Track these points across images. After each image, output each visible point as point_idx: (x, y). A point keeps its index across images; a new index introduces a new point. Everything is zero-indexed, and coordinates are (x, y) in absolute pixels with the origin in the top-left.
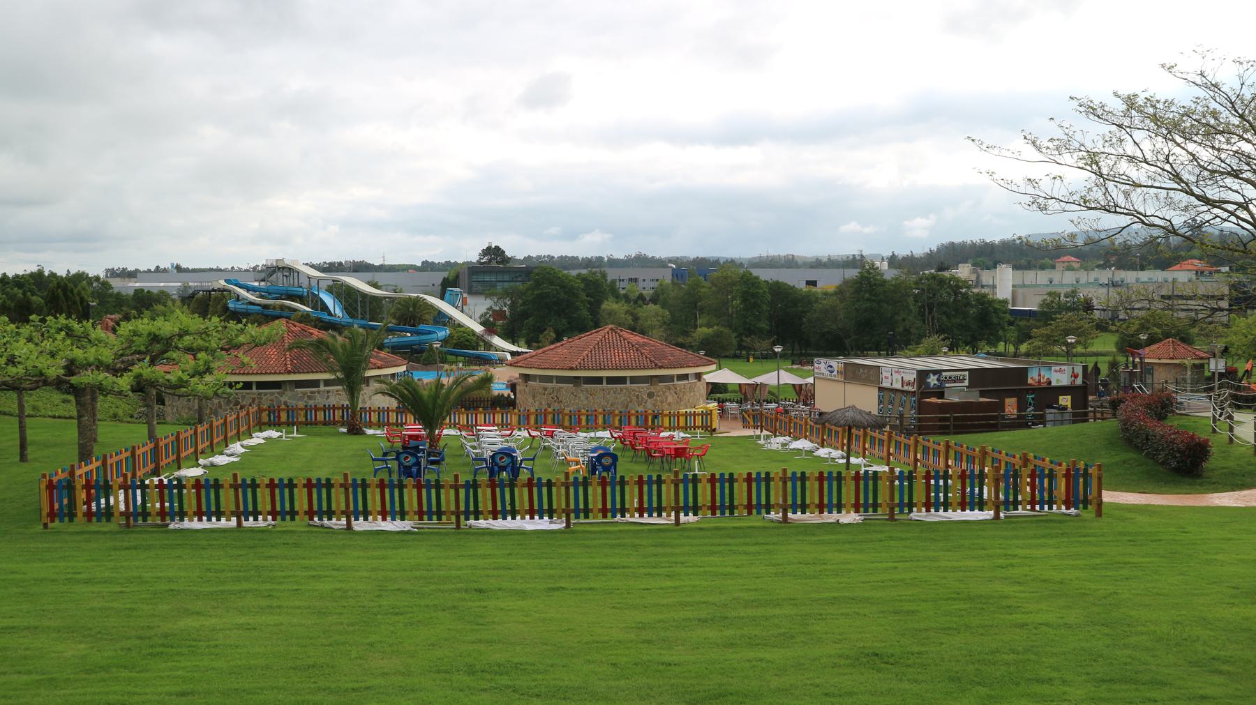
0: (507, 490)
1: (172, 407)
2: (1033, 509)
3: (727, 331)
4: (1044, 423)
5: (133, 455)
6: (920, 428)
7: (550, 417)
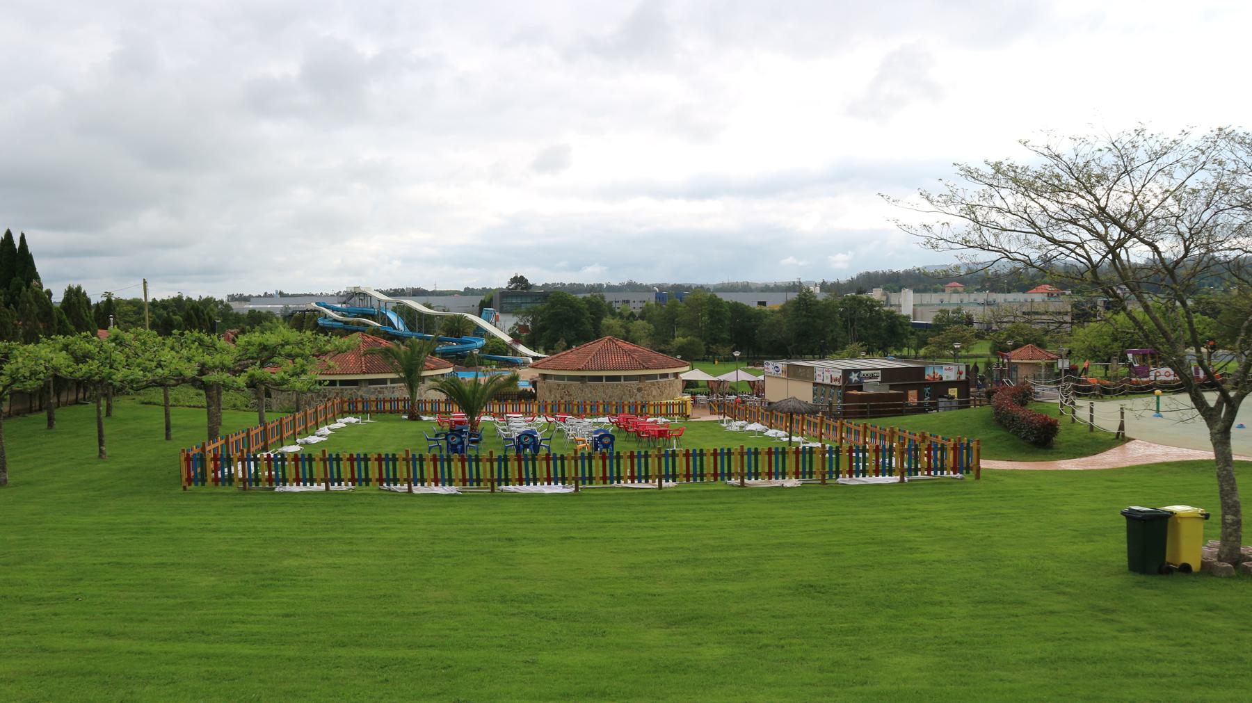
0: (530, 463)
1: (277, 399)
2: (929, 474)
3: (697, 340)
4: (937, 409)
5: (248, 434)
6: (845, 413)
7: (562, 407)
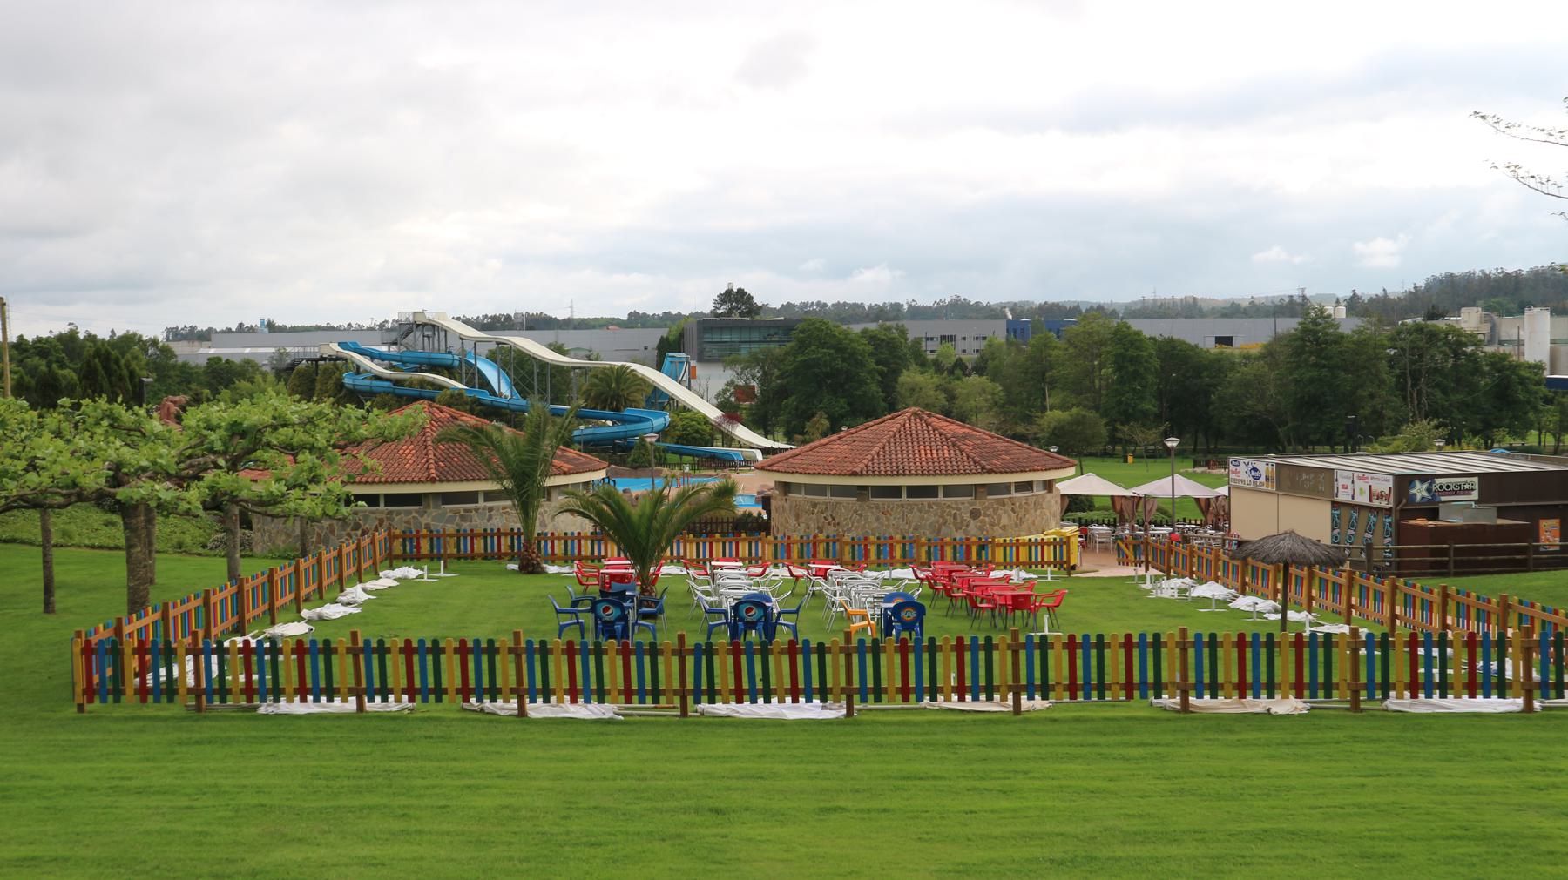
0: (758, 659)
1: (262, 532)
3: (1092, 415)
5: (206, 603)
6: (1399, 565)
7: (821, 548)
